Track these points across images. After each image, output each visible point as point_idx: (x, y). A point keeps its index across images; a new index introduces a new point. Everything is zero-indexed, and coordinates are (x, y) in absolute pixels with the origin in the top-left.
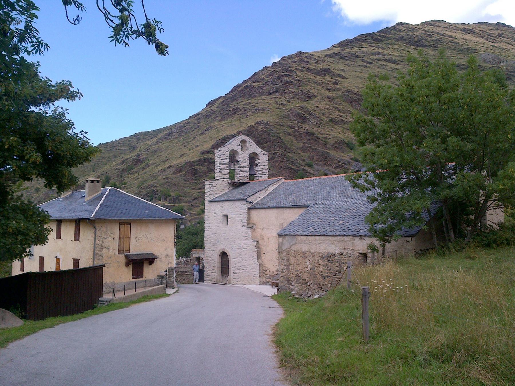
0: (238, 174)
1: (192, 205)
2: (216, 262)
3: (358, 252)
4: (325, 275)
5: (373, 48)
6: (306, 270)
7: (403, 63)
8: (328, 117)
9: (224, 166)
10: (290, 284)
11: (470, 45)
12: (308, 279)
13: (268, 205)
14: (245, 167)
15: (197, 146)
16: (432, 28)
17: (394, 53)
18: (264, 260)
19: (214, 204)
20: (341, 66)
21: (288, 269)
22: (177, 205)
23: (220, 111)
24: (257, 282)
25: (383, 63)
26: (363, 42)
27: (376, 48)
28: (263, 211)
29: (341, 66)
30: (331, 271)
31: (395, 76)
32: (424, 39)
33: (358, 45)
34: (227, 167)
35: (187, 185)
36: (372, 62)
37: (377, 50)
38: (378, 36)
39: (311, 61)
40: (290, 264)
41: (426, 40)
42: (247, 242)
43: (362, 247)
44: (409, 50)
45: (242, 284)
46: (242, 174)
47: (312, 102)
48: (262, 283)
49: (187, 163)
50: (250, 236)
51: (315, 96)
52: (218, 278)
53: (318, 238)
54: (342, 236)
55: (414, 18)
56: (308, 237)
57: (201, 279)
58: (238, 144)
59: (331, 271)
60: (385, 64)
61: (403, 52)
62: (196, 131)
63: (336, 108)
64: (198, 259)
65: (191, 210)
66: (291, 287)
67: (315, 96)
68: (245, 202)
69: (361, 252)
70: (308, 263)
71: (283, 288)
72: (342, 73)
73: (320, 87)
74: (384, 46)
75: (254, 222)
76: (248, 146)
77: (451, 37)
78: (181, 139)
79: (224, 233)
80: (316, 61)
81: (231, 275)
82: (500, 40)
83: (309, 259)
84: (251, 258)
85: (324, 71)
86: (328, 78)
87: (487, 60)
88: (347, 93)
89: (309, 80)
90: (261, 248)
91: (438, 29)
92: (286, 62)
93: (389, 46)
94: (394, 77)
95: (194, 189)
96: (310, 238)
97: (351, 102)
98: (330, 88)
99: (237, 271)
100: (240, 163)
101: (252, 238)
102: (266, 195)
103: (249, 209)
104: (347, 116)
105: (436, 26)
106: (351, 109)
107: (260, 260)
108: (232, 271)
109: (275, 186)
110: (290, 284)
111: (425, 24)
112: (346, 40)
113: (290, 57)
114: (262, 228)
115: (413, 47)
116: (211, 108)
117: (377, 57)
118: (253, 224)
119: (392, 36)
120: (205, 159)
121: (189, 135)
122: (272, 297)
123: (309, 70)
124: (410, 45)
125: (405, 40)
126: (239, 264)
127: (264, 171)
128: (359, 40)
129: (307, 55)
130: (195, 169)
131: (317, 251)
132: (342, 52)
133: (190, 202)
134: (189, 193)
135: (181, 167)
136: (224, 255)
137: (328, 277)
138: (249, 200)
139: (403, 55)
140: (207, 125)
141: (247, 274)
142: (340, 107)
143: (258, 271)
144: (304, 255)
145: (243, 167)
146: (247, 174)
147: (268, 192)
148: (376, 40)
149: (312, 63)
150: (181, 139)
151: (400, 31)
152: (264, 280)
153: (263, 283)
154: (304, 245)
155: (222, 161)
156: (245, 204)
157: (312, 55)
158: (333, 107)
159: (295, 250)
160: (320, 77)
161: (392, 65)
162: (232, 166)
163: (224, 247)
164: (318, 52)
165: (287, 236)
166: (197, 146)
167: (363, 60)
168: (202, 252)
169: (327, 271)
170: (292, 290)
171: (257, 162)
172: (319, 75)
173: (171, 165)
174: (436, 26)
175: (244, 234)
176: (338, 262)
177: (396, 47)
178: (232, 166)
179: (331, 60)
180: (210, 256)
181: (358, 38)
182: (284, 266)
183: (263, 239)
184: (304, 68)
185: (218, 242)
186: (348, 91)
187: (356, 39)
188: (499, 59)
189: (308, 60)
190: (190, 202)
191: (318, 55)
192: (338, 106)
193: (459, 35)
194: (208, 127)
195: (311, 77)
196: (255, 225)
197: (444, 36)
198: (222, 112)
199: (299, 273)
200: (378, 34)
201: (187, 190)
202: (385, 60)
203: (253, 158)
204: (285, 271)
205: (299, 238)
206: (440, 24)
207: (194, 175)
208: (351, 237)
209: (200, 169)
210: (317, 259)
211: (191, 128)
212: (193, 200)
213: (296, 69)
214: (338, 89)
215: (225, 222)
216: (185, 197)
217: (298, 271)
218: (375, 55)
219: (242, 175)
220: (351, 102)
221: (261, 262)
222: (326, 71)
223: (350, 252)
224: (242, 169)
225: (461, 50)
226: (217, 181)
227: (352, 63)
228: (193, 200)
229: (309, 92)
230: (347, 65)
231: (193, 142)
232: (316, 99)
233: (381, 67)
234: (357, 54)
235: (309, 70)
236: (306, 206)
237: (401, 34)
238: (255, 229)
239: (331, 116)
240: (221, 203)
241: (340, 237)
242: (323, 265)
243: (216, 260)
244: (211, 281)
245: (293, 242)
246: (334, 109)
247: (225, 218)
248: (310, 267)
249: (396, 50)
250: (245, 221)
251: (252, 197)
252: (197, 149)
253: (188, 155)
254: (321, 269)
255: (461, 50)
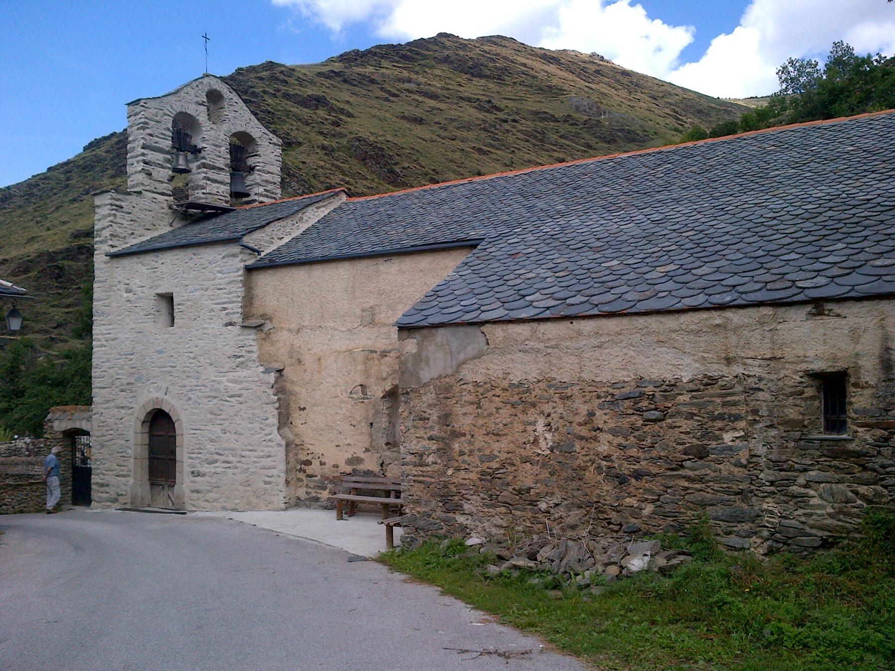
0: (197, 187)
1: (52, 339)
2: (132, 442)
3: (804, 366)
4: (626, 468)
5: (399, 70)
6: (529, 451)
7: (449, 101)
8: (322, 182)
9: (159, 157)
10: (457, 508)
11: (554, 82)
12: (540, 488)
13: (317, 253)
14: (221, 169)
15: (64, 223)
16: (494, 48)
17: (435, 83)
18: (301, 429)
19: (126, 262)
20: (345, 96)
21: (444, 451)
22: (19, 338)
23: (112, 159)
24: (279, 500)
25: (417, 97)
26: (382, 58)
27: (405, 72)
28: (300, 273)
29: (345, 96)
30: (654, 453)
31: (436, 120)
32: (482, 65)
33: (374, 63)
34: (168, 161)
35: (41, 299)
36: (398, 93)
37: (405, 74)
38: (408, 51)
39: (291, 80)
40: (456, 435)
41: (486, 66)
42: (242, 373)
43: (821, 349)
44: (459, 80)
45: (224, 509)
46: (213, 188)
47: (293, 153)
48: (293, 501)
49: (41, 255)
50: (254, 356)
51: (300, 144)
52: (139, 491)
53: (587, 326)
54: (721, 307)
55: (469, 28)
56: (542, 327)
57: (80, 488)
58: (200, 100)
59: (654, 453)
60: (420, 99)
61: (450, 82)
62: (61, 195)
63: (338, 167)
64: (73, 435)
65: (49, 347)
66: (461, 519)
67: (300, 144)
68: (235, 249)
69: (818, 366)
70: (540, 427)
71: (421, 523)
72: (347, 107)
73: (308, 129)
74: (417, 69)
75: (268, 311)
76: (228, 112)
77: (524, 65)
78: (30, 209)
79: (160, 352)
80: (301, 81)
81: (185, 482)
82: (597, 80)
83: (547, 408)
84: (257, 425)
85: (315, 100)
86: (321, 113)
87: (582, 109)
88: (357, 143)
89: (288, 113)
90: (291, 393)
91: (504, 50)
92: (245, 78)
93: (427, 70)
94: (436, 123)
95: (57, 306)
96: (551, 330)
97: (363, 160)
98: (325, 131)
99: (205, 468)
100: (203, 154)
101: (261, 360)
102: (297, 233)
103: (249, 270)
104: (356, 183)
105: (501, 45)
106: (364, 171)
107: (286, 430)
108: (187, 469)
109: (323, 212)
110: (457, 508)
111: (483, 40)
112: (353, 51)
113: (252, 69)
114: (294, 326)
115: (465, 76)
116: (94, 153)
117: (406, 86)
118: (264, 316)
119: (431, 53)
120: (80, 248)
121: (47, 201)
122: (382, 560)
123: (287, 96)
124: (460, 72)
125: (452, 62)
126: (210, 447)
127: (269, 187)
128: (375, 54)
129: (283, 69)
130: (58, 267)
131: (586, 376)
132: (346, 70)
133: (47, 332)
134: (45, 313)
135: (29, 261)
136: (159, 422)
137: (638, 475)
138: (248, 240)
139: (449, 87)
140: (85, 184)
141: (241, 477)
142: (345, 166)
143: (282, 467)
144: (522, 397)
145: (213, 168)
146: (224, 189)
147: (304, 227)
148: (404, 57)
149: (293, 84)
150: (30, 209)
151: (445, 47)
152: (301, 493)
153: (297, 503)
154: (519, 357)
155: (151, 141)
156: (235, 255)
157: (293, 70)
158: (333, 165)
159: (479, 379)
160: (307, 110)
161: (433, 103)
162: (181, 161)
163: (160, 395)
164: (303, 67)
165: (441, 331)
166: (64, 223)
167: (382, 89)
168: (86, 415)
169: (634, 452)
170: (465, 531)
171: (251, 161)
172: (306, 107)
173: (7, 257)
174: (501, 45)
175: (231, 351)
176: (691, 416)
177: (437, 72)
178: (181, 161)
179: (328, 82)
180: (112, 428)
181: (374, 50)
182: (426, 443)
183: (300, 361)
184: (279, 91)
185: (139, 379)
186: (359, 139)
187: (369, 52)
188: (598, 108)
189: (286, 78)
190: (47, 332)
191: (304, 71)
192: (341, 165)
193: (537, 65)
194: (87, 187)
195: (292, 109)
196: (271, 319)
197: (512, 62)
198: (116, 161)
199: (495, 465)
200: (408, 48)
201: (41, 307)
202: (420, 93)
203: (241, 148)
204: (430, 459)
205: (498, 333)
206: (506, 43)
207: (56, 278)
208: (767, 311)
209: (68, 265)
210: (584, 409)
211: (52, 189)
212: (54, 328)
213: (264, 92)
214: (340, 133)
215: (164, 317)
216: (37, 322)
217: (491, 457)
218: (403, 82)
219: (213, 189)
220: (363, 160)
221: (291, 436)
222: (319, 102)
223: (757, 371)
224: (211, 174)
225: (541, 89)
226: (134, 198)
227: (365, 92)
228: (54, 328)
229: (288, 134)
230: (356, 95)
231: (56, 215)
232: (302, 149)
233: (415, 104)
234: (373, 77)
235: (287, 96)
236: (471, 245)
237: (446, 53)
238: (268, 334)
239: (328, 180)
240: (149, 259)
241: (705, 315)
242: (614, 432)
243: (131, 436)
244: (115, 500)
245: (471, 351)
246: (333, 169)
247: (163, 306)
248: (547, 440)
249: (436, 78)
250: (236, 308)
251: (257, 235)
252: (64, 227)
253: (44, 240)
254: (603, 448)
255: (541, 89)
